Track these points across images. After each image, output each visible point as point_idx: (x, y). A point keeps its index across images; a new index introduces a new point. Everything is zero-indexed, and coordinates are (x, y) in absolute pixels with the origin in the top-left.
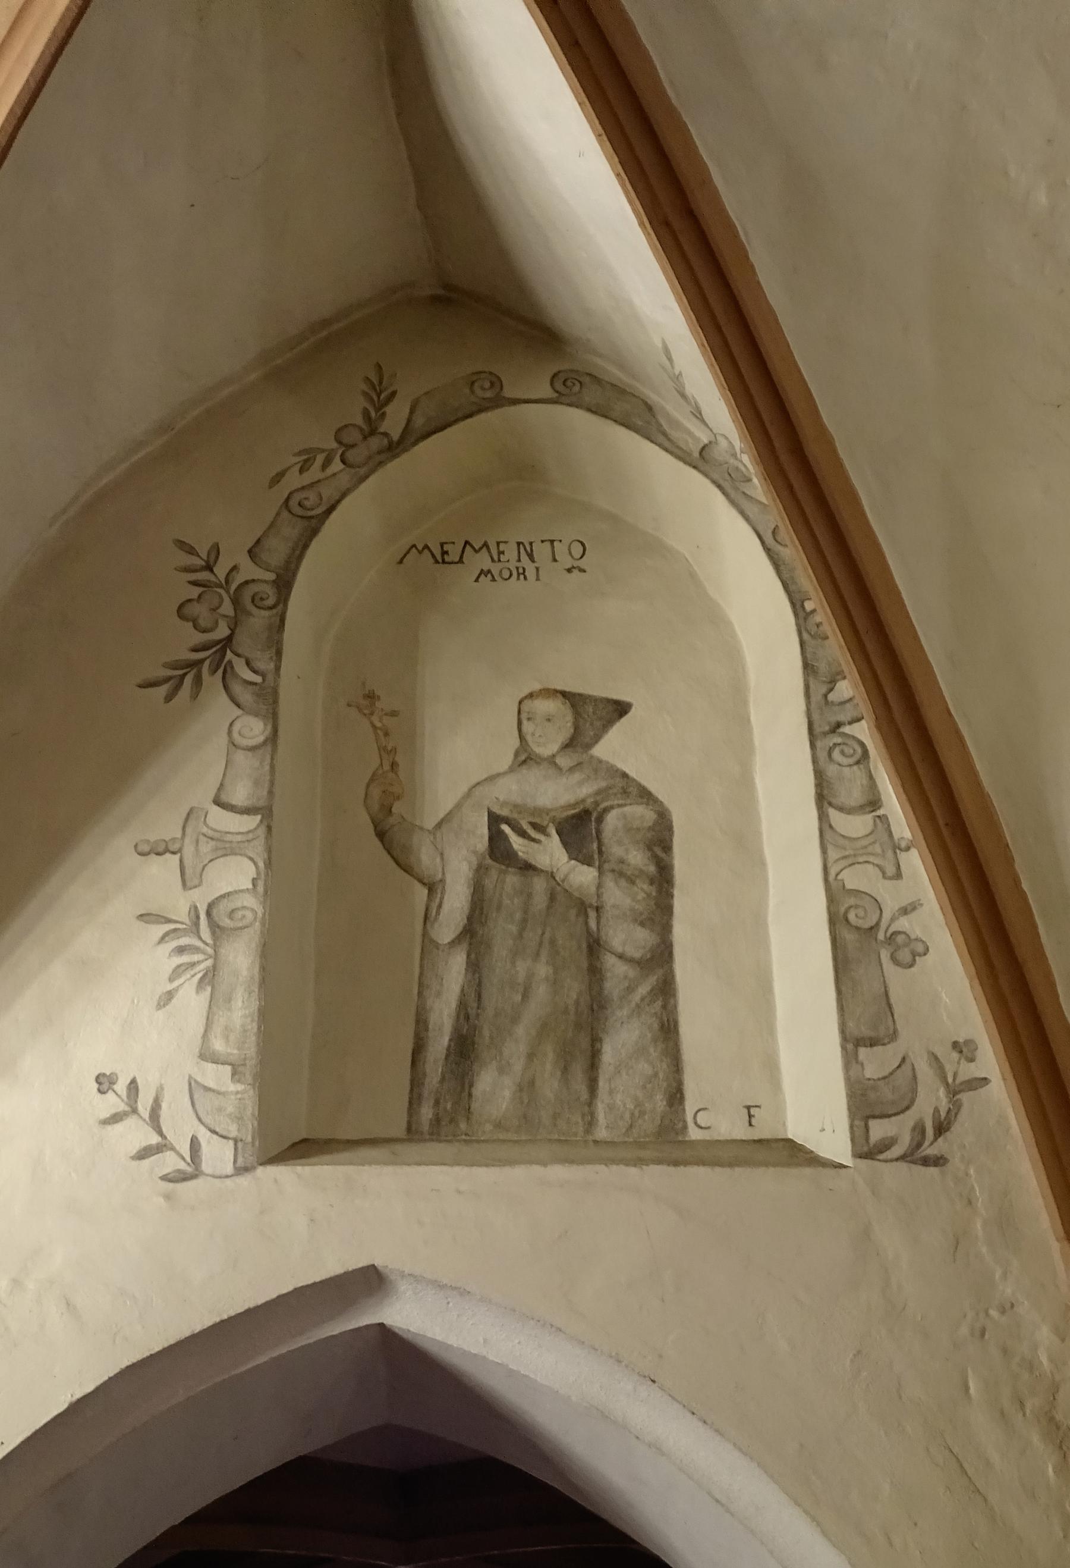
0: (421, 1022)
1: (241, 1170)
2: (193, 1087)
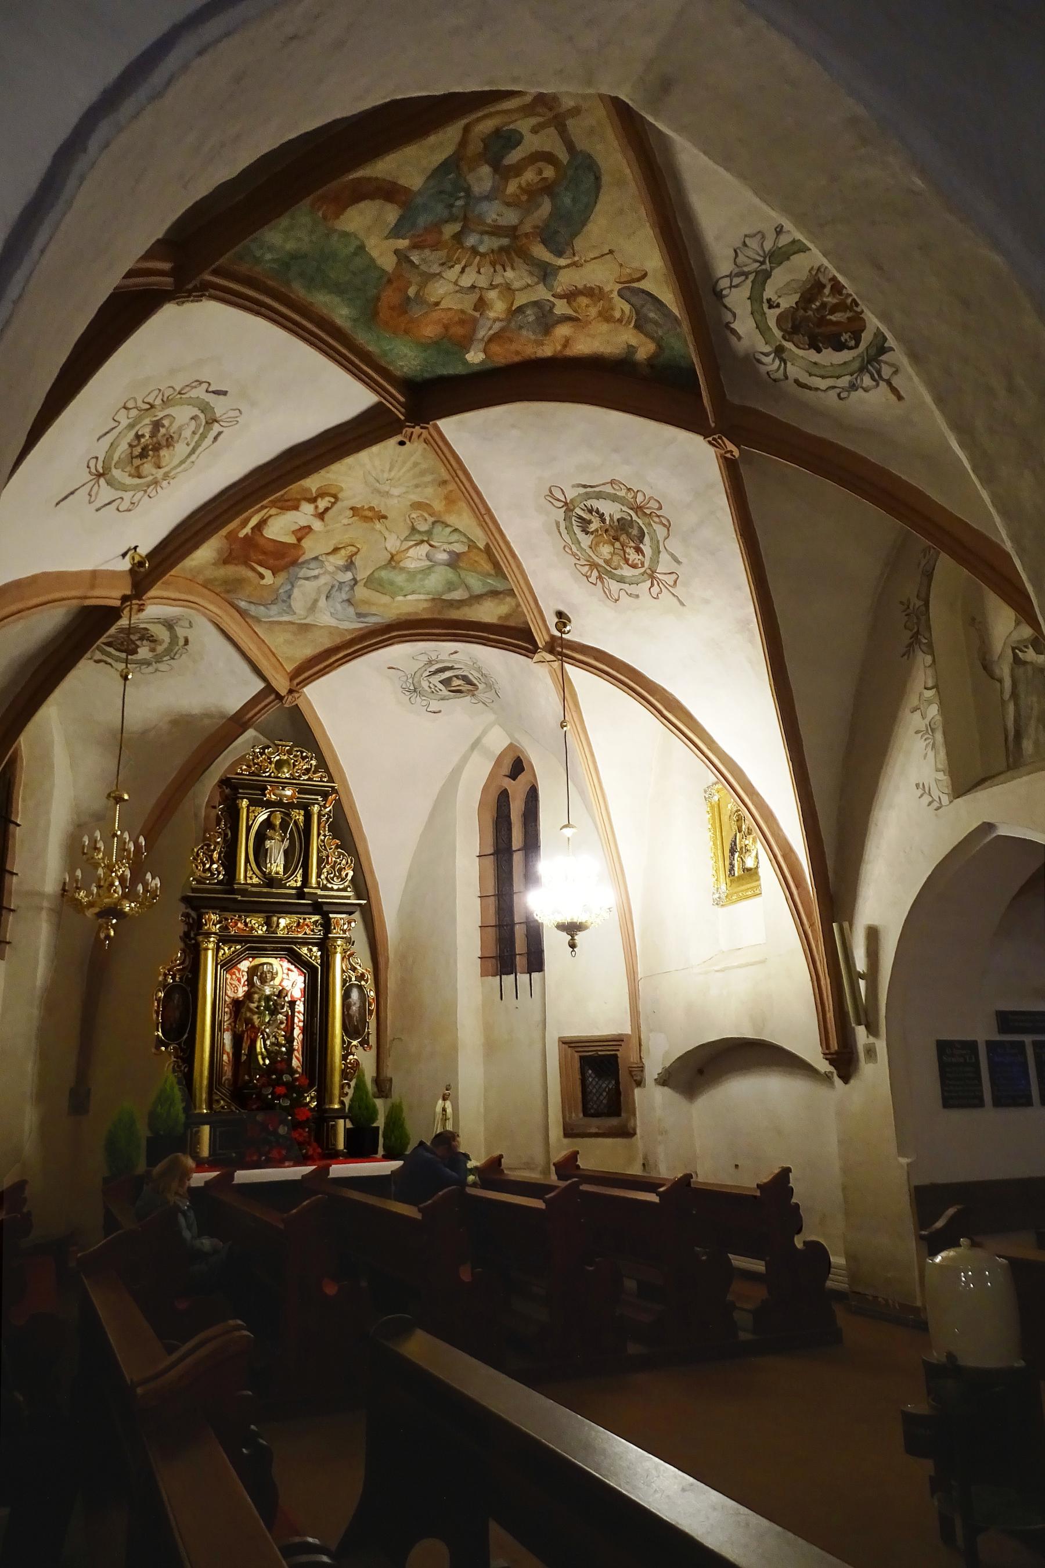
0: (1006, 730)
1: (951, 802)
2: (936, 780)
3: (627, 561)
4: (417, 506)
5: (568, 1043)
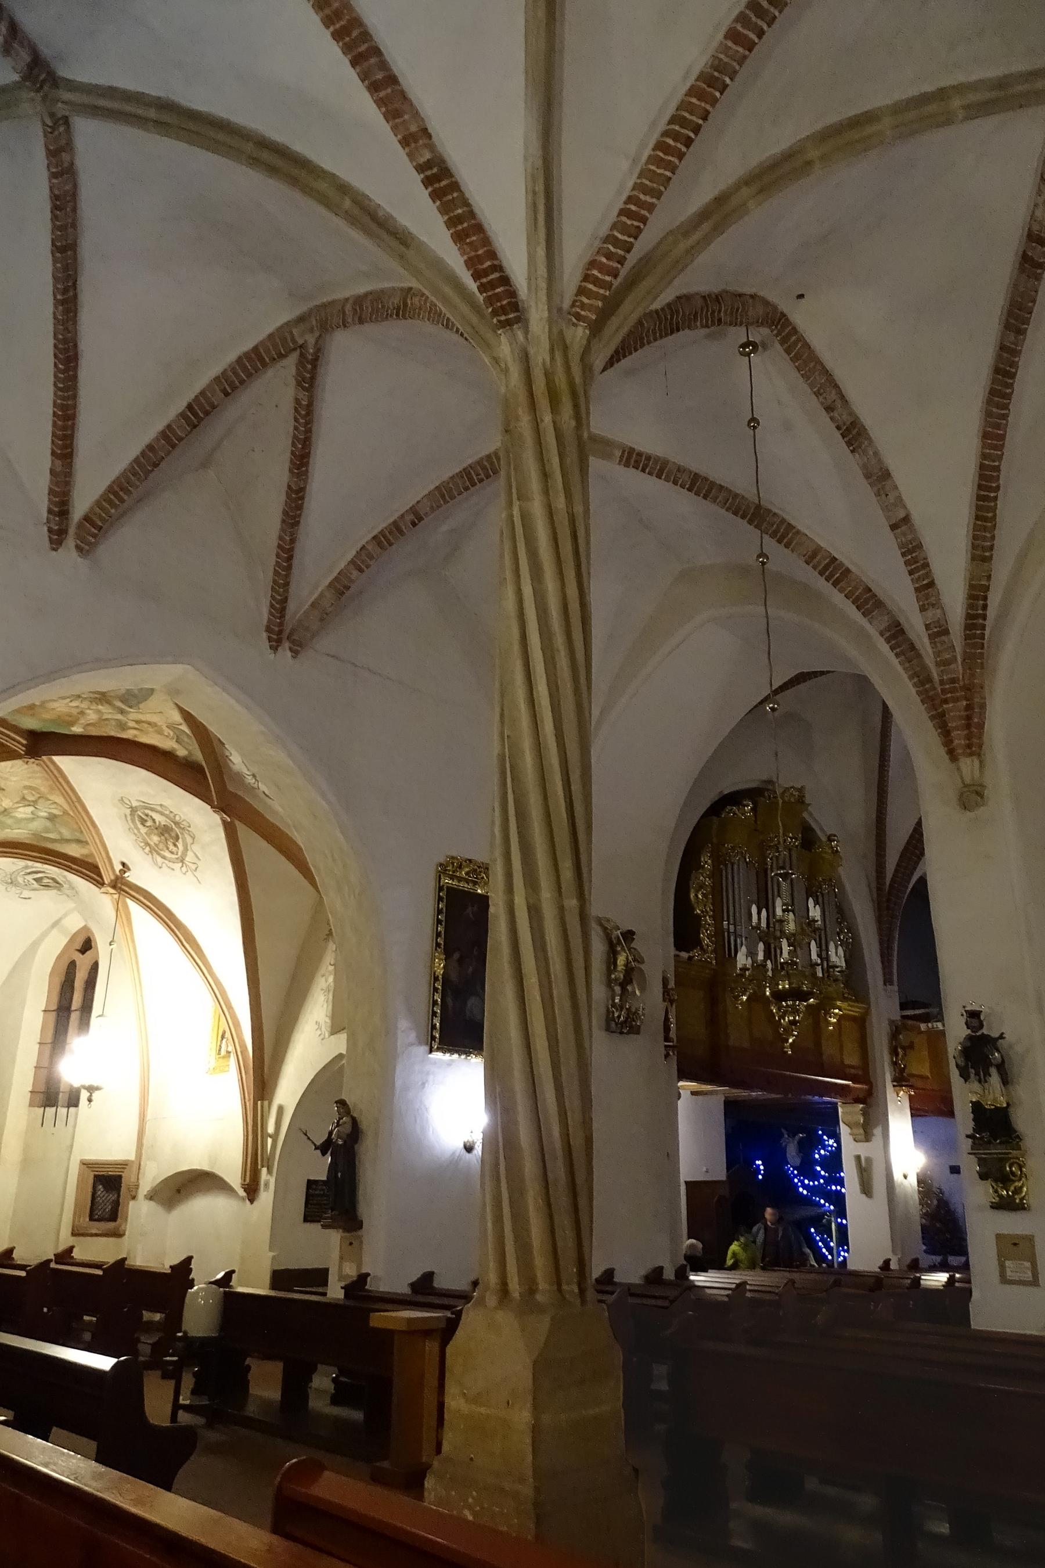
3: (168, 849)
4: (26, 787)
5: (86, 1164)
